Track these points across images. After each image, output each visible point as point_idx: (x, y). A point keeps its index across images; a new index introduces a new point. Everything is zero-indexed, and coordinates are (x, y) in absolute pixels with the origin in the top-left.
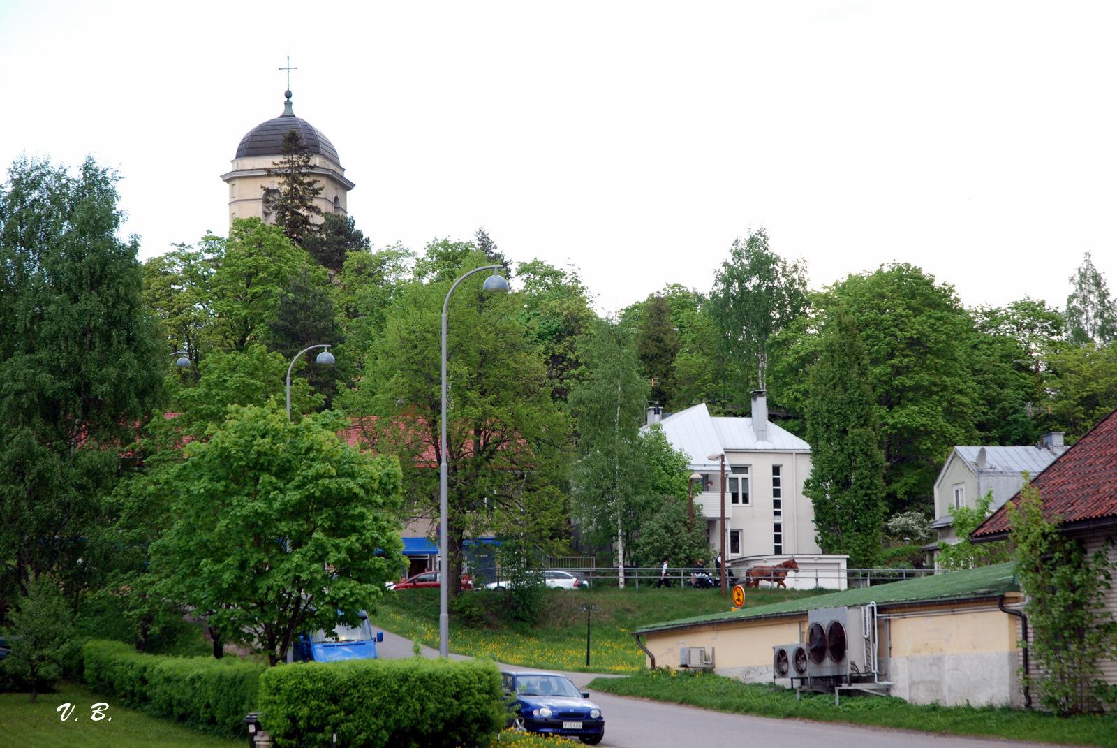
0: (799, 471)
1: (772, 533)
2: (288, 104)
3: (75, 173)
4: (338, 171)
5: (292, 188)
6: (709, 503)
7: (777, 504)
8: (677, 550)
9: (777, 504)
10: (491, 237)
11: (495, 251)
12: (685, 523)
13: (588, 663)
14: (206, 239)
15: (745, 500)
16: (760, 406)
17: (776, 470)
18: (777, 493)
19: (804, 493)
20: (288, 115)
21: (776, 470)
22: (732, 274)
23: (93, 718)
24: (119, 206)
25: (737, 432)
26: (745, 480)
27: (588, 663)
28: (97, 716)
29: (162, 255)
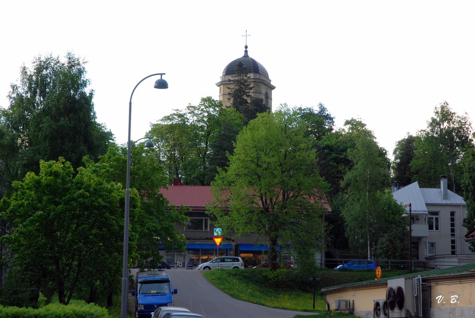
0: (462, 214)
1: (450, 244)
2: (246, 52)
3: (64, 60)
4: (268, 81)
5: (240, 87)
6: (419, 230)
7: (453, 230)
8: (395, 252)
9: (453, 230)
10: (325, 106)
11: (327, 113)
12: (400, 238)
13: (314, 307)
14: (188, 107)
15: (437, 228)
16: (443, 183)
17: (452, 214)
18: (453, 225)
19: (463, 225)
20: (246, 55)
21: (452, 214)
22: (434, 123)
23: (452, 302)
24: (85, 77)
25: (436, 195)
26: (437, 219)
27: (314, 307)
28: (453, 301)
29: (169, 115)
